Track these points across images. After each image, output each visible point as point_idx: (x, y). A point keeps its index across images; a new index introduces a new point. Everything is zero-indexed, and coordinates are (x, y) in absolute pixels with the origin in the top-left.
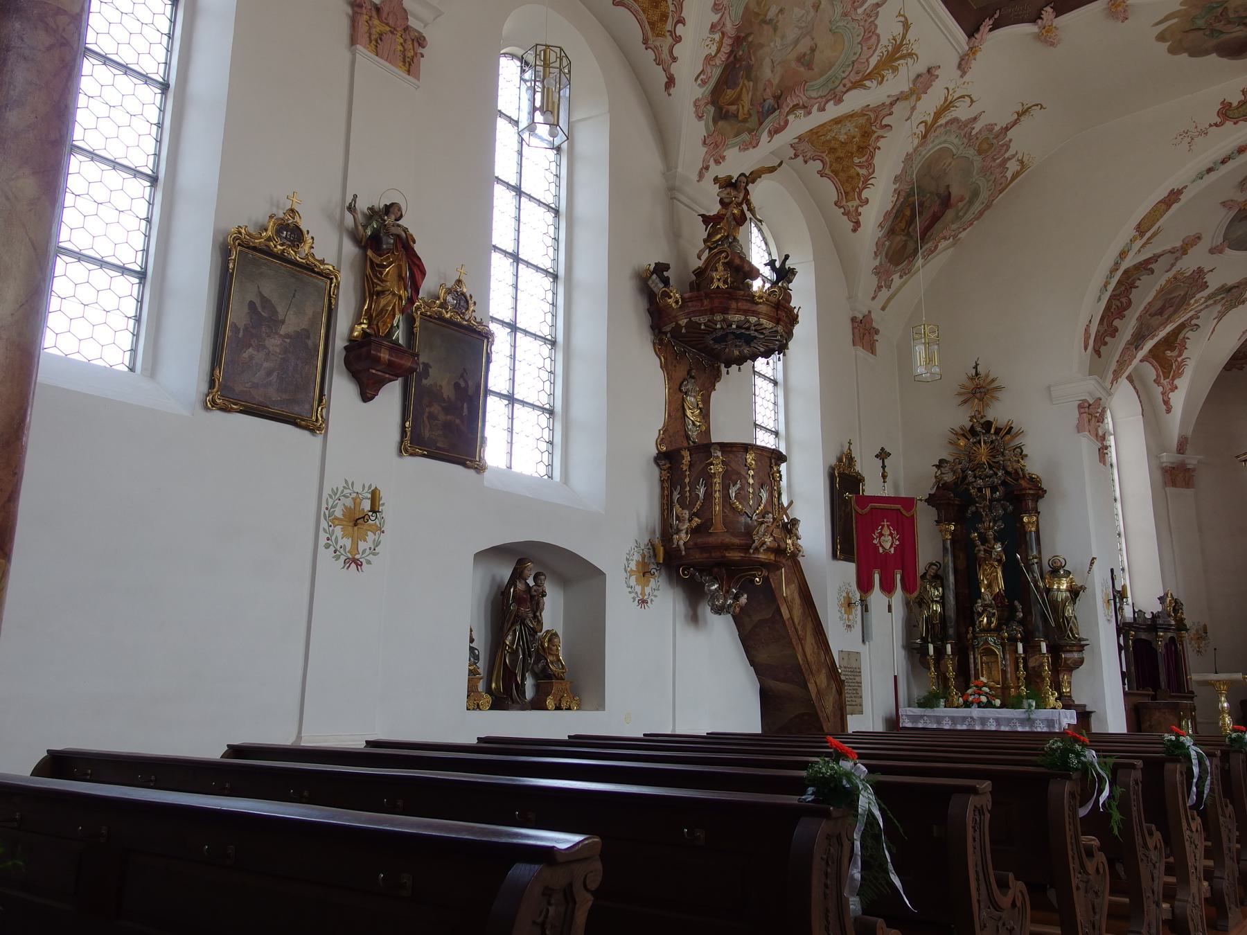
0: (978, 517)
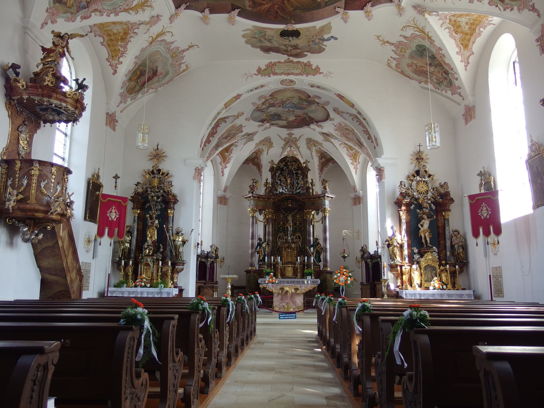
0: (150, 208)
